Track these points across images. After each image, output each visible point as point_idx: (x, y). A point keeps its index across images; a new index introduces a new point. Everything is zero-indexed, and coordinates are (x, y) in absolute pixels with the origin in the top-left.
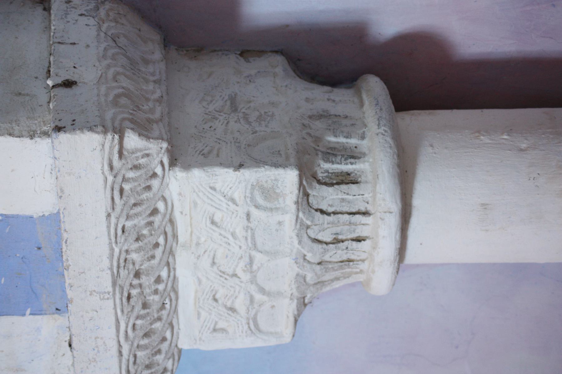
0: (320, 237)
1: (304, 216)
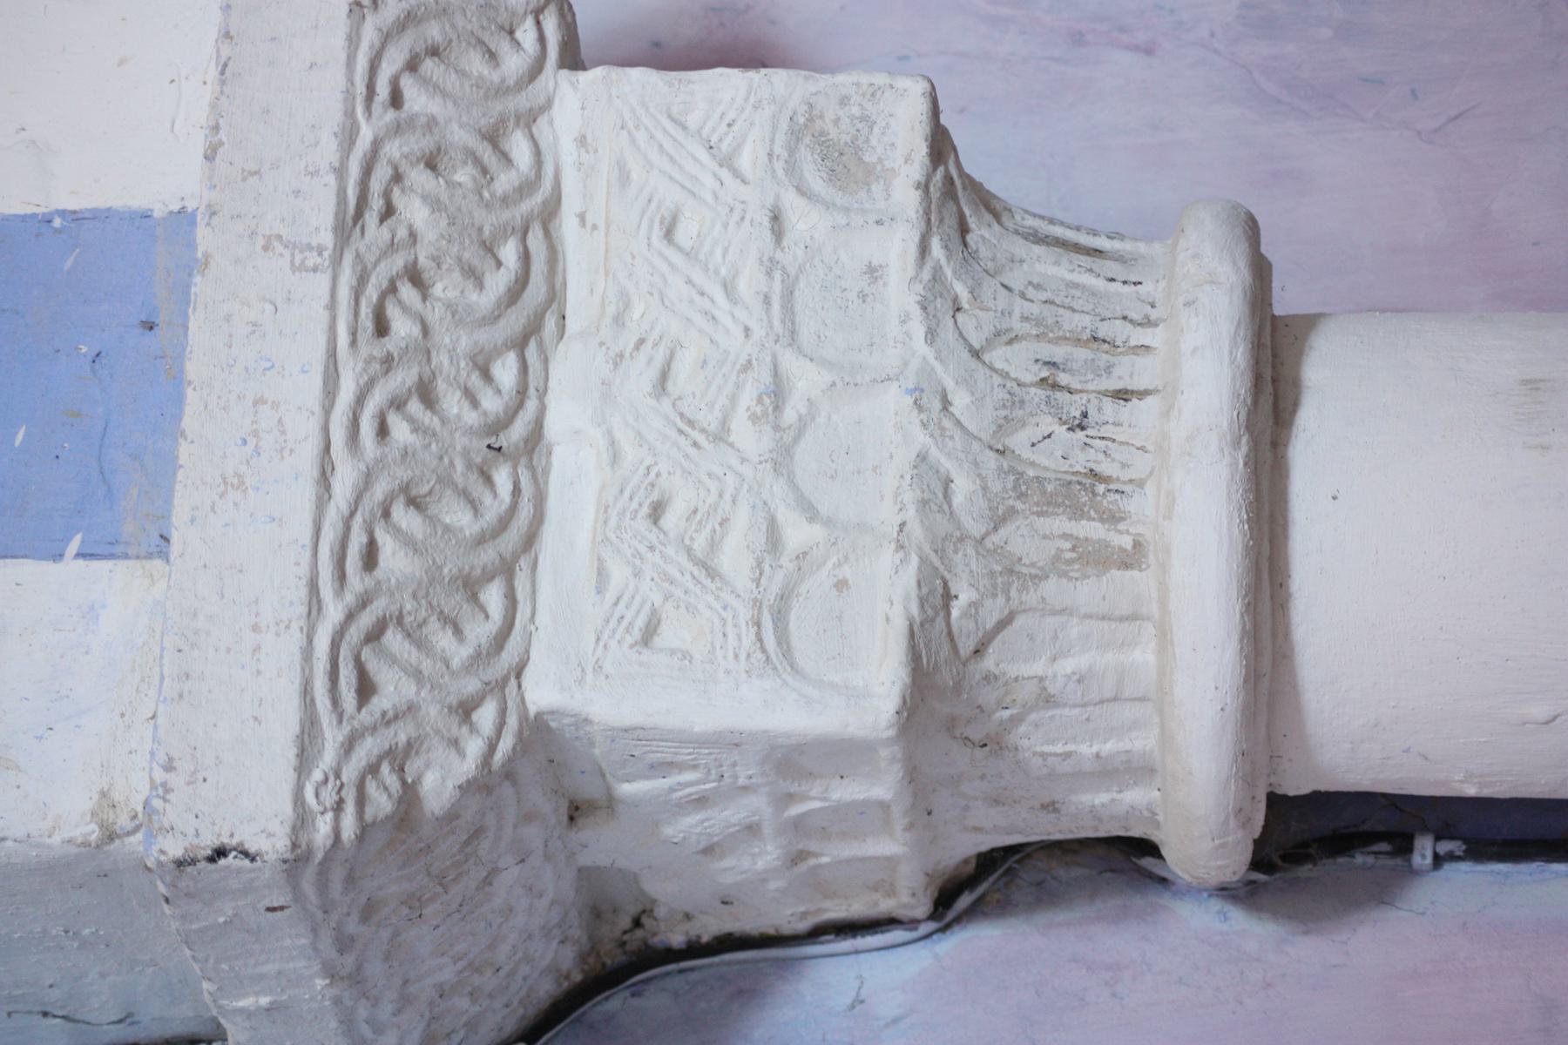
1: (948, 262)
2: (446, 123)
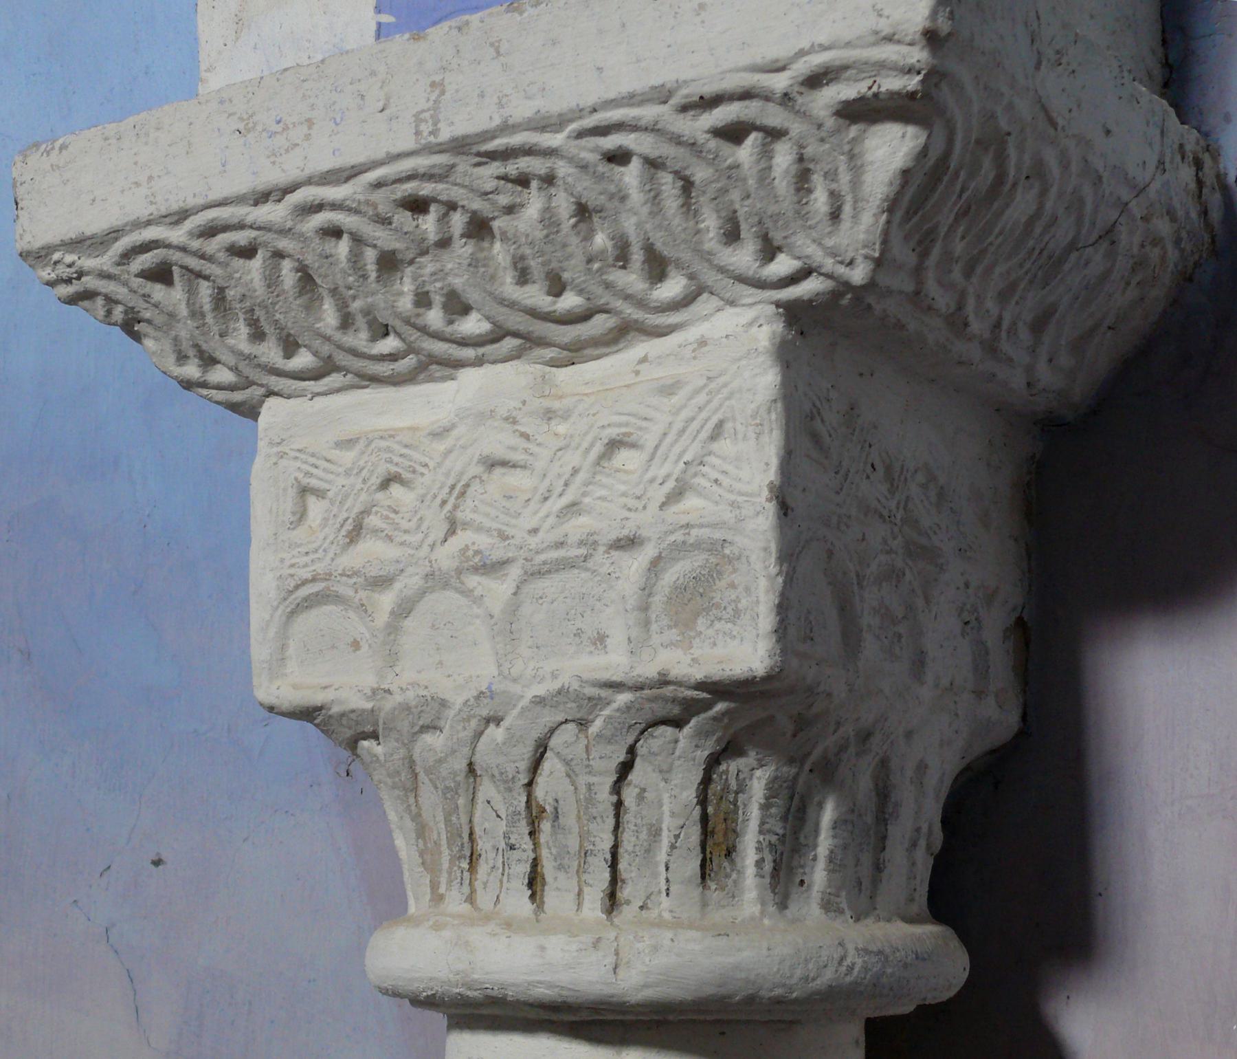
0: (550, 764)
1: (618, 710)
2: (629, 210)
